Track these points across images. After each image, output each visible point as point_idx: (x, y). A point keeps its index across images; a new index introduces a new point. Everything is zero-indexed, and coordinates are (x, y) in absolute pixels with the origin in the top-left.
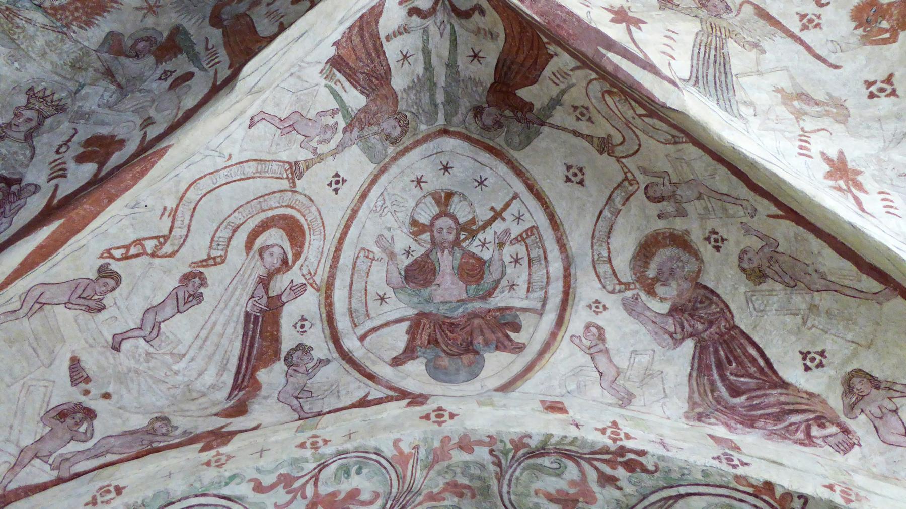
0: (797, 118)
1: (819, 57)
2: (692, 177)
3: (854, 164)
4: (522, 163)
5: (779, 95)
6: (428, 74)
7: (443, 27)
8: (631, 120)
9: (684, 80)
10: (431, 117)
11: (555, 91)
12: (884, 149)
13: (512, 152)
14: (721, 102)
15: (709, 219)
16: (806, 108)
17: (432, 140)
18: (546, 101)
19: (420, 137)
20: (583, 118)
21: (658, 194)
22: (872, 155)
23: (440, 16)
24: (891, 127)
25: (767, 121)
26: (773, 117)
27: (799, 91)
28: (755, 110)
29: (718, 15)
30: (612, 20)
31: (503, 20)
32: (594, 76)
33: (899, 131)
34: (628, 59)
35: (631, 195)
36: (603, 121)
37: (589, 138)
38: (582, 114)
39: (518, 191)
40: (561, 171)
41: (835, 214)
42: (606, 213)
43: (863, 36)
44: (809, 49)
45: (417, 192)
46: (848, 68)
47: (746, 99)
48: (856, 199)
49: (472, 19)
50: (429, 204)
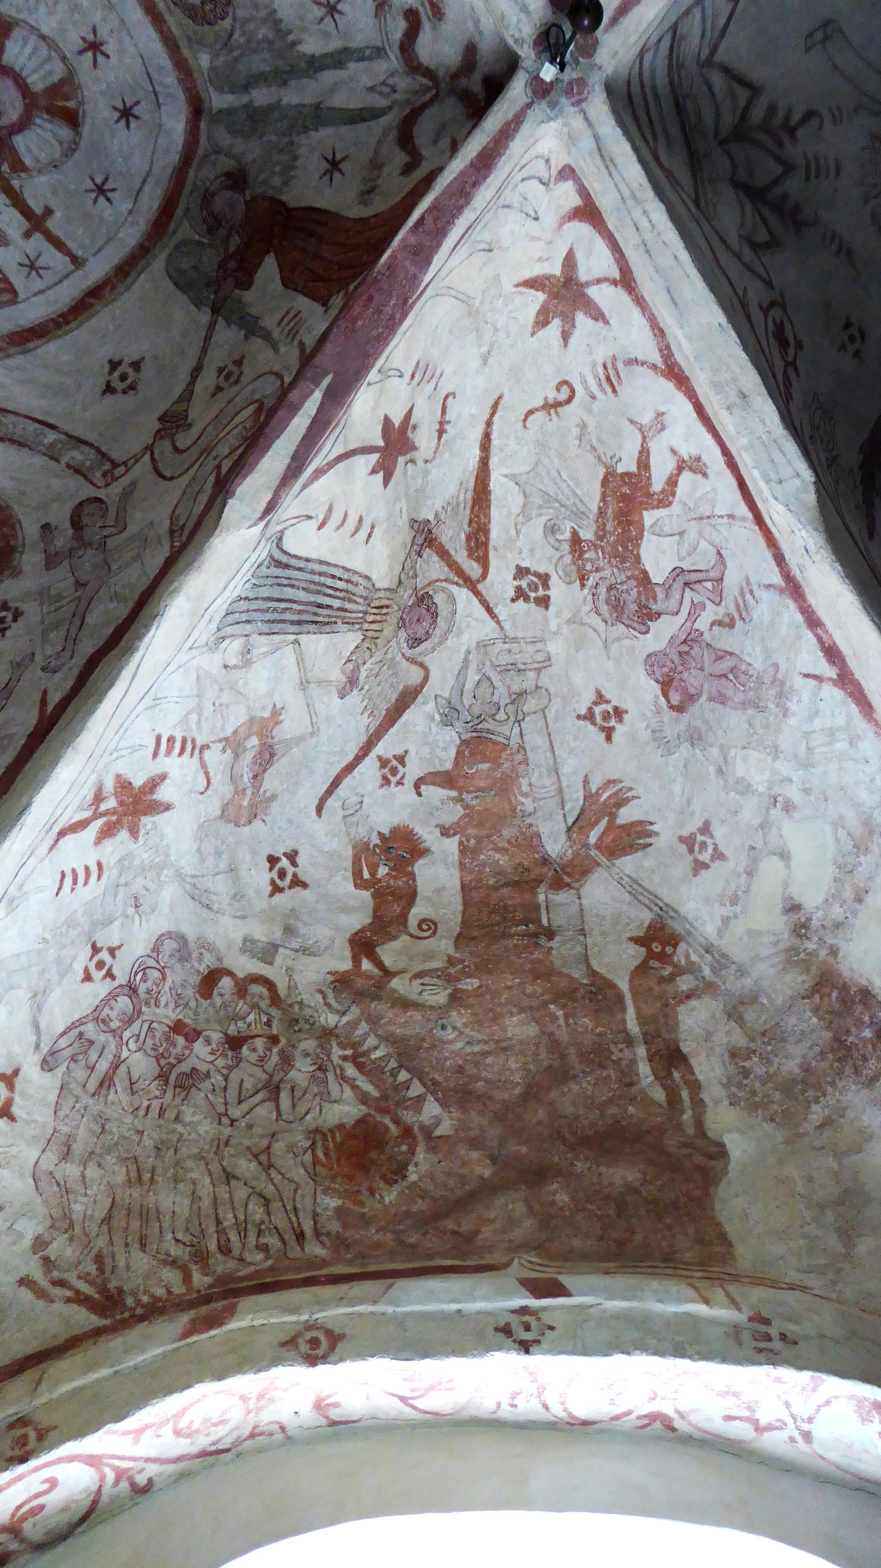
0: (226, 739)
1: (336, 783)
2: (114, 567)
3: (150, 826)
4: (142, 277)
5: (267, 714)
6: (303, 65)
7: (386, 90)
8: (214, 454)
9: (280, 539)
10: (224, 80)
11: (269, 322)
12: (180, 876)
13: (163, 256)
14: (244, 605)
15: (41, 605)
16: (248, 758)
17: (180, 81)
18: (252, 311)
19: (186, 52)
20: (222, 378)
21: (86, 520)
22: (168, 856)
23: (403, 83)
24: (221, 886)
25: (216, 686)
26: (226, 698)
27: (278, 749)
28: (235, 667)
29: (402, 623)
30: (387, 421)
31: (392, 209)
32: (287, 380)
33: (214, 898)
34: (310, 428)
35: (85, 477)
36: (213, 413)
37: (188, 394)
38: (228, 377)
39: (89, 266)
40: (131, 352)
41: (44, 782)
42: (51, 437)
43: (367, 844)
44: (350, 768)
45: (72, 41)
46: (318, 827)
47: (255, 652)
48: (83, 824)
49: (397, 149)
50: (48, 67)
